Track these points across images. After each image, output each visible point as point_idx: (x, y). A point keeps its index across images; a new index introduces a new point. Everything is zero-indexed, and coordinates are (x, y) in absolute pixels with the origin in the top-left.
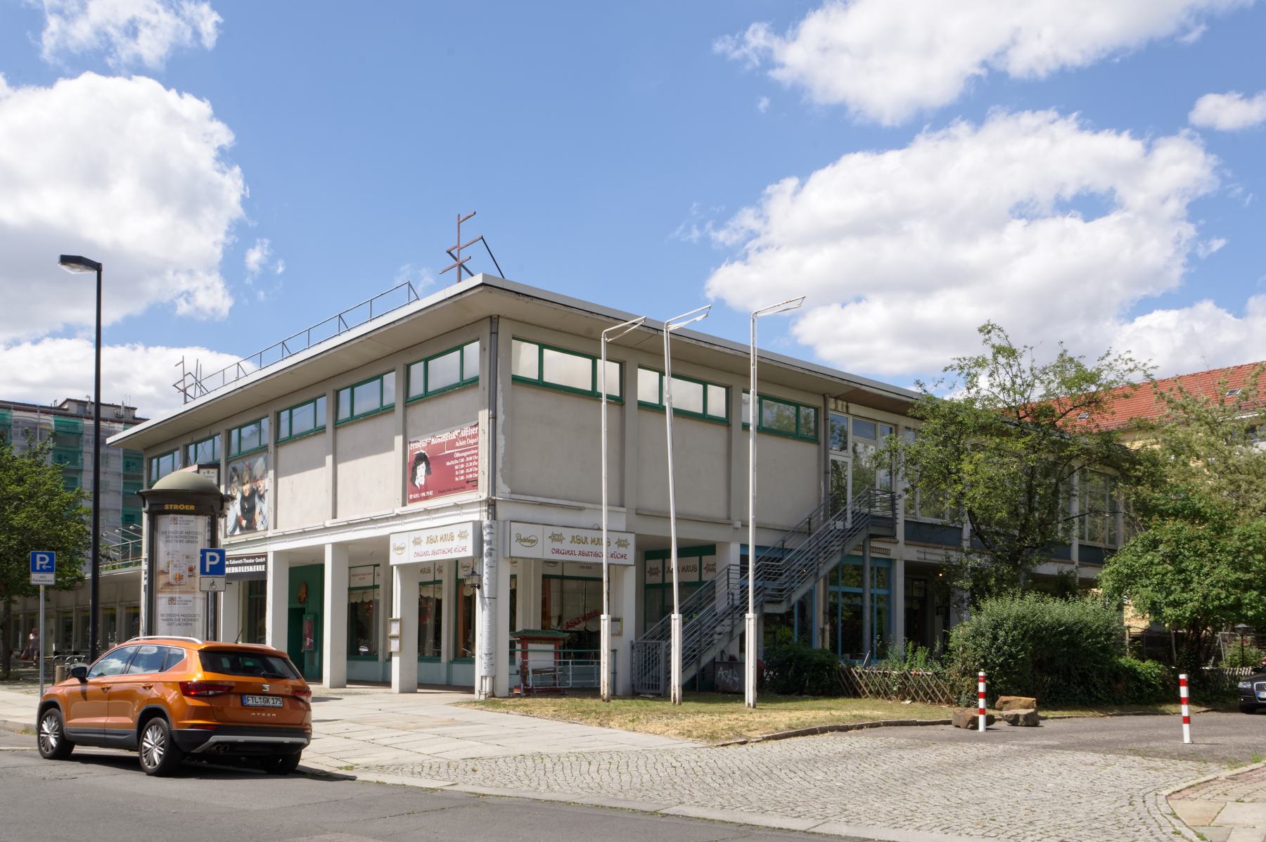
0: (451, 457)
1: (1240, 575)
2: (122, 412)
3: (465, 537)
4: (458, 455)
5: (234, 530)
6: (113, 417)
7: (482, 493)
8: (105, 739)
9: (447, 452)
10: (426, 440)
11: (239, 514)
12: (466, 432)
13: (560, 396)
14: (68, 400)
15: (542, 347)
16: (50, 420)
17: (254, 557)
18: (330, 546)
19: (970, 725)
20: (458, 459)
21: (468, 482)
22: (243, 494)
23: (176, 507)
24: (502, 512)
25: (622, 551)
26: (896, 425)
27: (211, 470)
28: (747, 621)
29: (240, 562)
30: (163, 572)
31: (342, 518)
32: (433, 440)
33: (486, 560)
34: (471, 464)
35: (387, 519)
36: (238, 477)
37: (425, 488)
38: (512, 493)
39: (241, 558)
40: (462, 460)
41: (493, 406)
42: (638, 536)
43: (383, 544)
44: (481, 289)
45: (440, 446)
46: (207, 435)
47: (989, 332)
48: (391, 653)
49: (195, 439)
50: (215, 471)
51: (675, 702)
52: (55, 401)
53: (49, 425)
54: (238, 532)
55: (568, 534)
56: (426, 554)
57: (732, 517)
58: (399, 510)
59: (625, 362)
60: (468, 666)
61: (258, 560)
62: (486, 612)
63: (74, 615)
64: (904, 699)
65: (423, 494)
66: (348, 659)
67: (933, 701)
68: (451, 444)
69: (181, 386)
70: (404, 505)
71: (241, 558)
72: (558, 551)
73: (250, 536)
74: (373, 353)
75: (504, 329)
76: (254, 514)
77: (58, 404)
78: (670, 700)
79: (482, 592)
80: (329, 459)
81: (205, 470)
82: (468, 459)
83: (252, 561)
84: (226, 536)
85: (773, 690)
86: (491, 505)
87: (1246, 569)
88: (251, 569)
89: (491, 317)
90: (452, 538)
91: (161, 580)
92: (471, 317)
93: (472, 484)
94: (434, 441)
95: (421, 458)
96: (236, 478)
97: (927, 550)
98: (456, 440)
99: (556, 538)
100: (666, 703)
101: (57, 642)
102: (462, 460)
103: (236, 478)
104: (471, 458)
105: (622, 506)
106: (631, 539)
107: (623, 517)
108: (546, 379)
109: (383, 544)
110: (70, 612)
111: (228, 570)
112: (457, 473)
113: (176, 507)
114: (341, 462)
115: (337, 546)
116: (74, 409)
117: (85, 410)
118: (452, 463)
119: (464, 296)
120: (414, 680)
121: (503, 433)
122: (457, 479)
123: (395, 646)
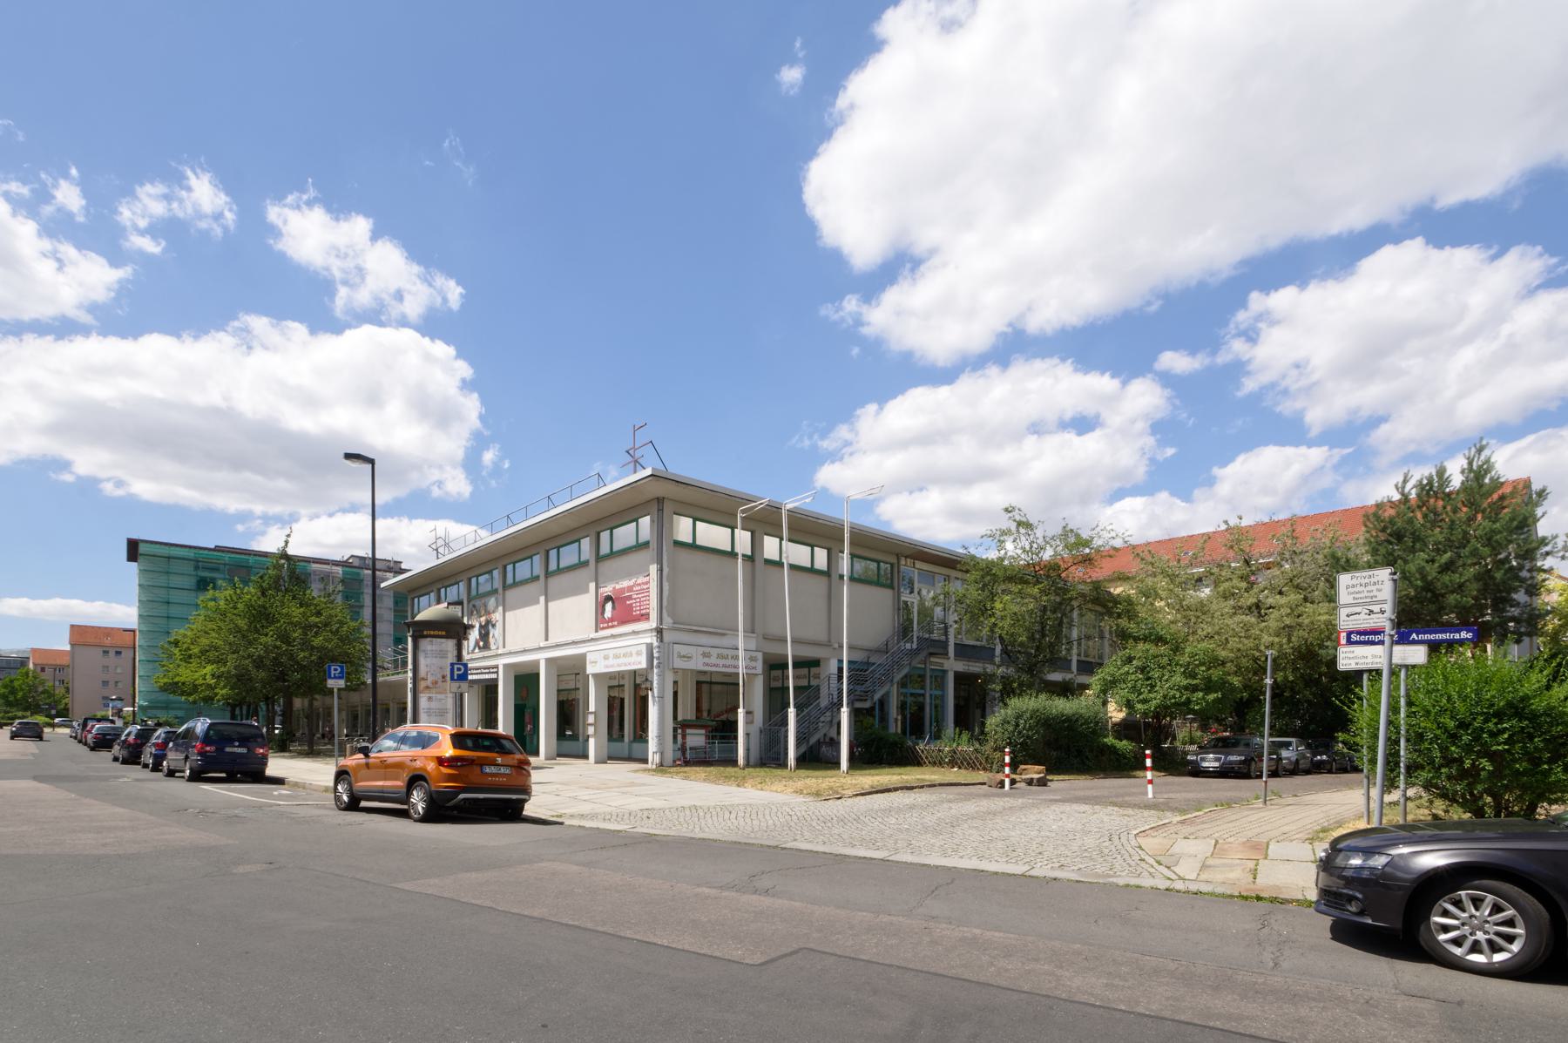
0: (630, 598)
2: (392, 565)
3: (641, 654)
4: (635, 596)
5: (474, 649)
7: (653, 623)
11: (478, 637)
14: (352, 556)
16: (339, 570)
23: (432, 633)
24: (667, 636)
26: (948, 576)
27: (457, 607)
29: (479, 671)
30: (423, 679)
33: (655, 670)
35: (584, 642)
37: (611, 620)
40: (638, 600)
41: (660, 562)
42: (764, 654)
43: (582, 658)
44: (651, 478)
50: (460, 607)
53: (338, 573)
54: (477, 650)
57: (833, 641)
60: (643, 745)
61: (492, 670)
62: (656, 708)
63: (359, 708)
64: (953, 767)
65: (610, 624)
68: (630, 589)
69: (434, 546)
70: (596, 631)
73: (486, 653)
75: (668, 507)
77: (345, 559)
80: (542, 599)
84: (468, 653)
85: (858, 762)
87: (1194, 676)
88: (487, 676)
89: (658, 498)
91: (422, 685)
94: (618, 587)
95: (608, 598)
96: (475, 612)
97: (970, 663)
102: (638, 600)
103: (475, 612)
105: (753, 632)
106: (760, 656)
107: (754, 640)
108: (698, 542)
109: (582, 658)
110: (357, 706)
111: (470, 677)
113: (432, 633)
114: (551, 601)
115: (549, 661)
116: (357, 563)
119: (638, 483)
120: (605, 754)
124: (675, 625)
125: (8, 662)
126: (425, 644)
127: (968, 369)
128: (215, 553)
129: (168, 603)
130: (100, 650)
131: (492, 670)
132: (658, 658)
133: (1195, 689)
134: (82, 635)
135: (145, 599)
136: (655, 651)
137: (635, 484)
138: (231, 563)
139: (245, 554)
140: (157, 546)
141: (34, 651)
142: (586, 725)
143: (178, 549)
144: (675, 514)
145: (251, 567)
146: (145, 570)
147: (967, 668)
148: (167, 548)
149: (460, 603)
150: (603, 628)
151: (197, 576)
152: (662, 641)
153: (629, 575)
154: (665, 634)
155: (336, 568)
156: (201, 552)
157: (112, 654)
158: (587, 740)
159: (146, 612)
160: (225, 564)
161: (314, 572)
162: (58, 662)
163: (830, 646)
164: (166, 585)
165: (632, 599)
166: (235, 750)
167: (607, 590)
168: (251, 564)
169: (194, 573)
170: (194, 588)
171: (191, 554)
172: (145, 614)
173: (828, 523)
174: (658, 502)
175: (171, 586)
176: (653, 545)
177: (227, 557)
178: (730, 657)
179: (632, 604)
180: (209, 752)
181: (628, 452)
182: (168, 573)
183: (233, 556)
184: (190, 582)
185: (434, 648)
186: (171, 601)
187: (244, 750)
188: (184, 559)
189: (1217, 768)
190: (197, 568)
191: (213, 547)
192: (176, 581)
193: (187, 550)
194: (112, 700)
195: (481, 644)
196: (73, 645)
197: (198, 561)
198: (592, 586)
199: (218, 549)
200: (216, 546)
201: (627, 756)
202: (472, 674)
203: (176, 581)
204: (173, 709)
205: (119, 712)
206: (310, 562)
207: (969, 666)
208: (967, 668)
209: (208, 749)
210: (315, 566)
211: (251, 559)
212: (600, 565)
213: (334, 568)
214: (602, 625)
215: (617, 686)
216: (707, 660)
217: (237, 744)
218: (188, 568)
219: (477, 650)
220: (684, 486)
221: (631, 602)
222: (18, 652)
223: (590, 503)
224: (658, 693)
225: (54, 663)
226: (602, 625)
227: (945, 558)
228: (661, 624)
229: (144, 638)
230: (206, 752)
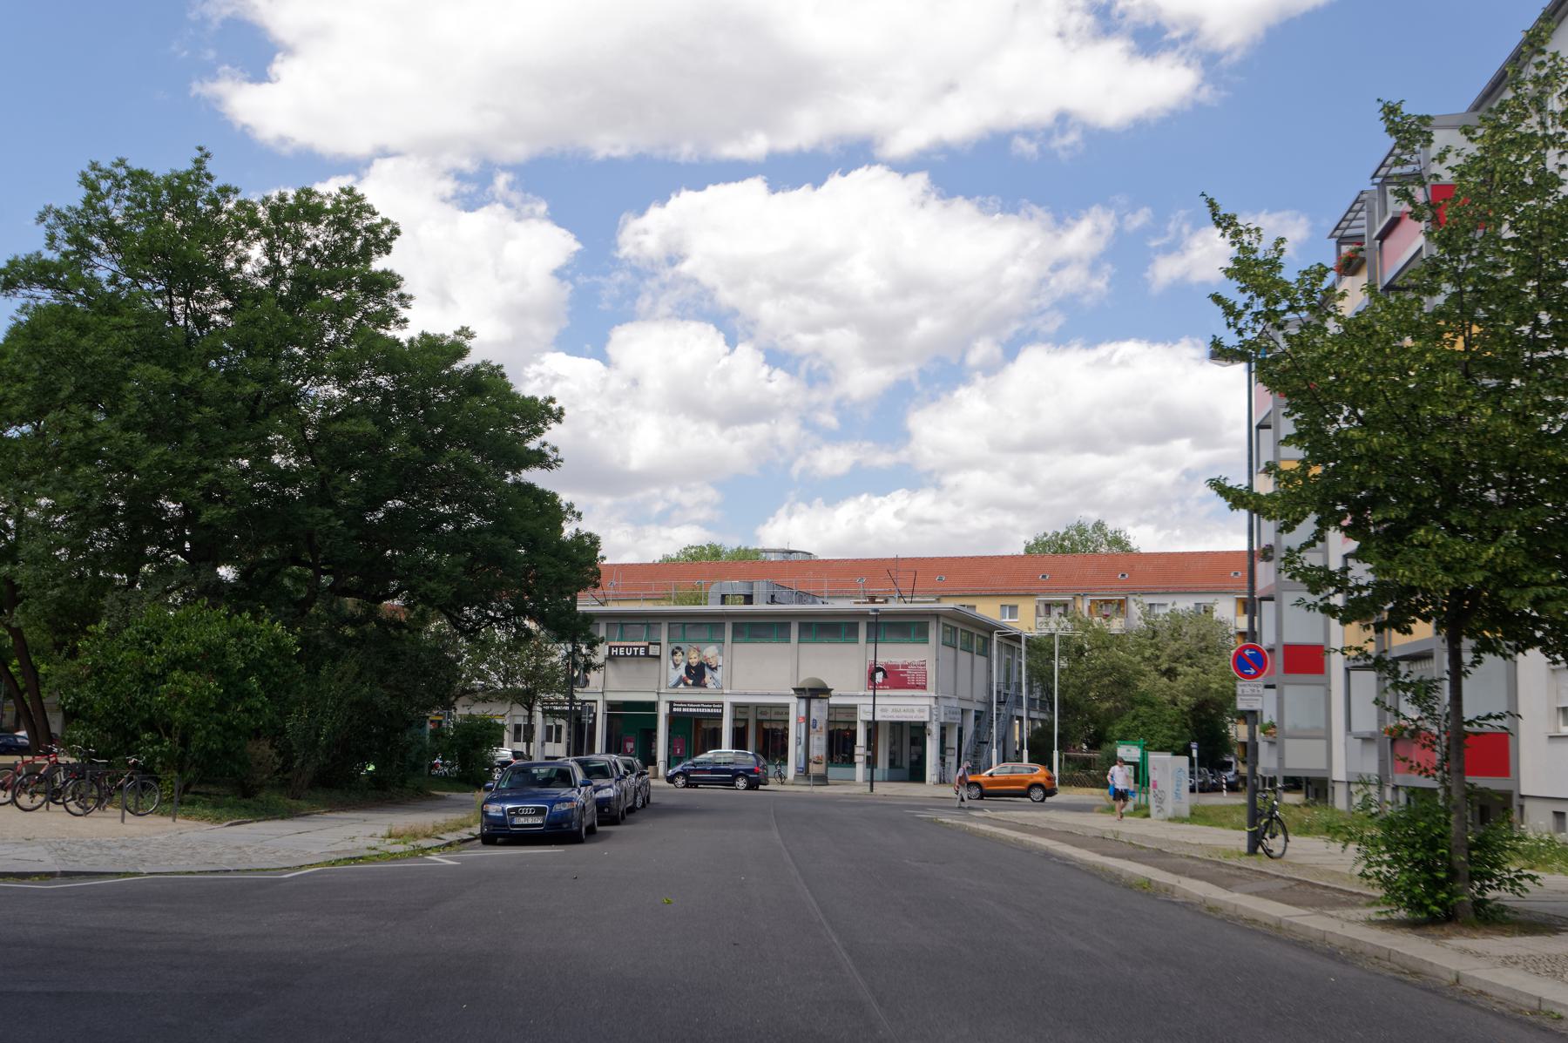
0: (905, 672)
11: (684, 675)
17: (686, 703)
25: (922, 714)
37: (883, 684)
54: (682, 686)
93: (924, 687)
216: (884, 714)
219: (682, 686)
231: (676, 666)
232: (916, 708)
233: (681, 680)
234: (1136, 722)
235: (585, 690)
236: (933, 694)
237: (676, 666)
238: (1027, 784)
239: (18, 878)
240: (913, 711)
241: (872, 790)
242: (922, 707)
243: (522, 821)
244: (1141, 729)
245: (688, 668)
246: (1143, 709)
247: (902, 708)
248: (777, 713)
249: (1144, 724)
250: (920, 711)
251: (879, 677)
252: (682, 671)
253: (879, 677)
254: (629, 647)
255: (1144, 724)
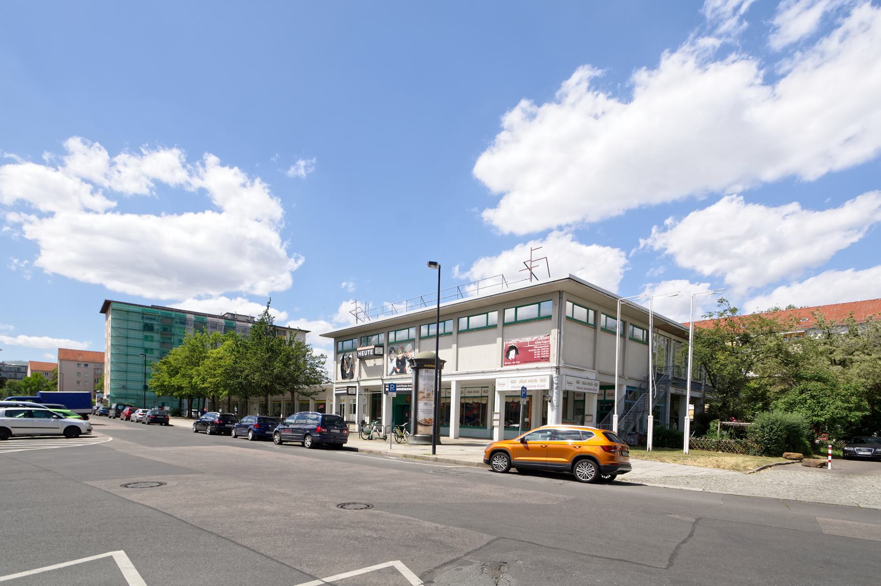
0: (532, 348)
1: (846, 405)
2: (249, 319)
3: (597, 386)
4: (536, 347)
5: (392, 373)
6: (246, 321)
7: (553, 362)
8: (546, 467)
9: (529, 346)
10: (516, 340)
11: (395, 366)
12: (542, 337)
13: (583, 326)
14: (227, 313)
15: (574, 304)
16: (223, 321)
17: (407, 385)
18: (455, 382)
19: (819, 466)
20: (536, 349)
21: (542, 358)
22: (397, 358)
23: (429, 366)
24: (562, 371)
25: (543, 383)
26: (670, 338)
27: (380, 348)
28: (685, 420)
29: (400, 386)
30: (421, 392)
31: (460, 371)
32: (520, 340)
33: (555, 391)
34: (544, 351)
35: (492, 372)
36: (395, 351)
37: (515, 360)
38: (565, 364)
39: (401, 385)
40: (539, 349)
41: (559, 327)
42: (600, 382)
43: (493, 383)
44: (567, 280)
45: (526, 343)
46: (376, 333)
47: (722, 302)
48: (493, 426)
49: (367, 335)
50: (382, 348)
51: (649, 451)
52: (274, 317)
53: (222, 323)
54: (394, 373)
55: (581, 380)
56: (581, 388)
57: (625, 374)
58: (499, 368)
59: (597, 311)
60: (448, 428)
61: (409, 386)
62: (554, 413)
63: (239, 403)
64: (718, 451)
65: (514, 363)
66: (460, 427)
67: (733, 452)
68: (532, 343)
69: (354, 312)
70: (502, 367)
71: (401, 385)
72: (578, 388)
73: (404, 376)
74: (485, 304)
75: (565, 296)
76: (405, 366)
77: (223, 315)
78: (646, 450)
79: (553, 403)
80: (454, 346)
81: (378, 348)
82: (542, 349)
83: (407, 386)
84: (387, 375)
85: (657, 445)
86: (558, 368)
87: (848, 402)
88: (405, 389)
89: (560, 291)
90: (592, 385)
91: (420, 396)
92: (552, 290)
93: (547, 359)
94: (520, 341)
95: (512, 348)
96: (393, 352)
97: (678, 389)
98: (535, 341)
99: (578, 382)
100: (643, 451)
101: (283, 414)
102: (539, 349)
103: (393, 352)
104: (544, 349)
105: (594, 369)
106: (598, 383)
107: (594, 374)
108: (574, 317)
109: (493, 383)
110: (238, 402)
111: (397, 389)
112: (535, 355)
113: (429, 366)
114: (460, 347)
115: (457, 382)
116: (230, 317)
117: (234, 318)
118: (532, 350)
119: (555, 282)
120: (458, 435)
121: (563, 339)
122: (535, 357)
123: (496, 423)
124: (566, 365)
125: (10, 368)
126: (423, 372)
127: (111, 212)
128: (152, 309)
129: (127, 338)
130: (76, 363)
131: (409, 386)
132: (557, 384)
133: (850, 410)
134: (65, 355)
135: (114, 335)
136: (554, 380)
137: (553, 283)
138: (163, 315)
139: (171, 311)
140: (122, 305)
141: (31, 362)
142: (492, 420)
143: (133, 307)
144: (567, 301)
145: (174, 318)
146: (115, 319)
147: (675, 391)
148: (127, 306)
149: (382, 346)
150: (507, 365)
151: (143, 322)
152: (559, 374)
153: (533, 335)
154: (561, 370)
155: (221, 320)
156: (146, 309)
157: (82, 365)
158: (493, 429)
159: (115, 342)
160: (159, 316)
161: (208, 321)
162: (45, 369)
163: (624, 377)
164: (126, 327)
165: (534, 349)
166: (335, 431)
167: (513, 342)
168: (173, 317)
169: (142, 321)
170: (142, 329)
171: (140, 310)
172: (115, 344)
173: (634, 307)
174: (560, 293)
175: (129, 328)
176: (555, 317)
177: (160, 312)
178: (527, 381)
179: (533, 352)
180: (324, 432)
181: (524, 263)
182: (127, 320)
183: (164, 311)
184: (139, 326)
185: (428, 375)
186: (129, 336)
187: (338, 431)
188: (136, 312)
189: (870, 455)
190: (143, 318)
191: (150, 306)
192: (132, 325)
193: (139, 307)
194: (98, 393)
195: (398, 370)
196: (60, 360)
197: (144, 314)
198: (499, 340)
199: (153, 307)
200: (152, 306)
201: (489, 437)
202: (398, 387)
203: (132, 325)
204: (129, 398)
205: (101, 400)
206: (206, 316)
207: (676, 390)
208: (675, 391)
209: (324, 430)
210: (209, 319)
211: (173, 314)
212: (505, 328)
213: (220, 320)
214: (506, 363)
215: (480, 397)
216: (514, 385)
217: (336, 428)
218: (138, 318)
219: (394, 373)
220: (580, 284)
221: (532, 350)
222: (15, 362)
223: (521, 290)
224: (557, 403)
225: (42, 369)
226: (506, 363)
227: (676, 328)
228: (559, 364)
229: (114, 358)
230: (323, 432)
231: (392, 360)
232: (538, 378)
233: (394, 370)
234: (804, 396)
235: (352, 380)
236: (555, 365)
237: (392, 360)
238: (572, 456)
239: (596, 460)
240: (536, 381)
241: (434, 452)
242: (543, 377)
243: (862, 453)
244: (809, 401)
245: (398, 360)
246: (812, 385)
247: (528, 379)
248: (469, 392)
249: (813, 397)
250: (541, 380)
251: (512, 353)
252: (394, 364)
253: (512, 353)
254: (366, 350)
255: (813, 397)
